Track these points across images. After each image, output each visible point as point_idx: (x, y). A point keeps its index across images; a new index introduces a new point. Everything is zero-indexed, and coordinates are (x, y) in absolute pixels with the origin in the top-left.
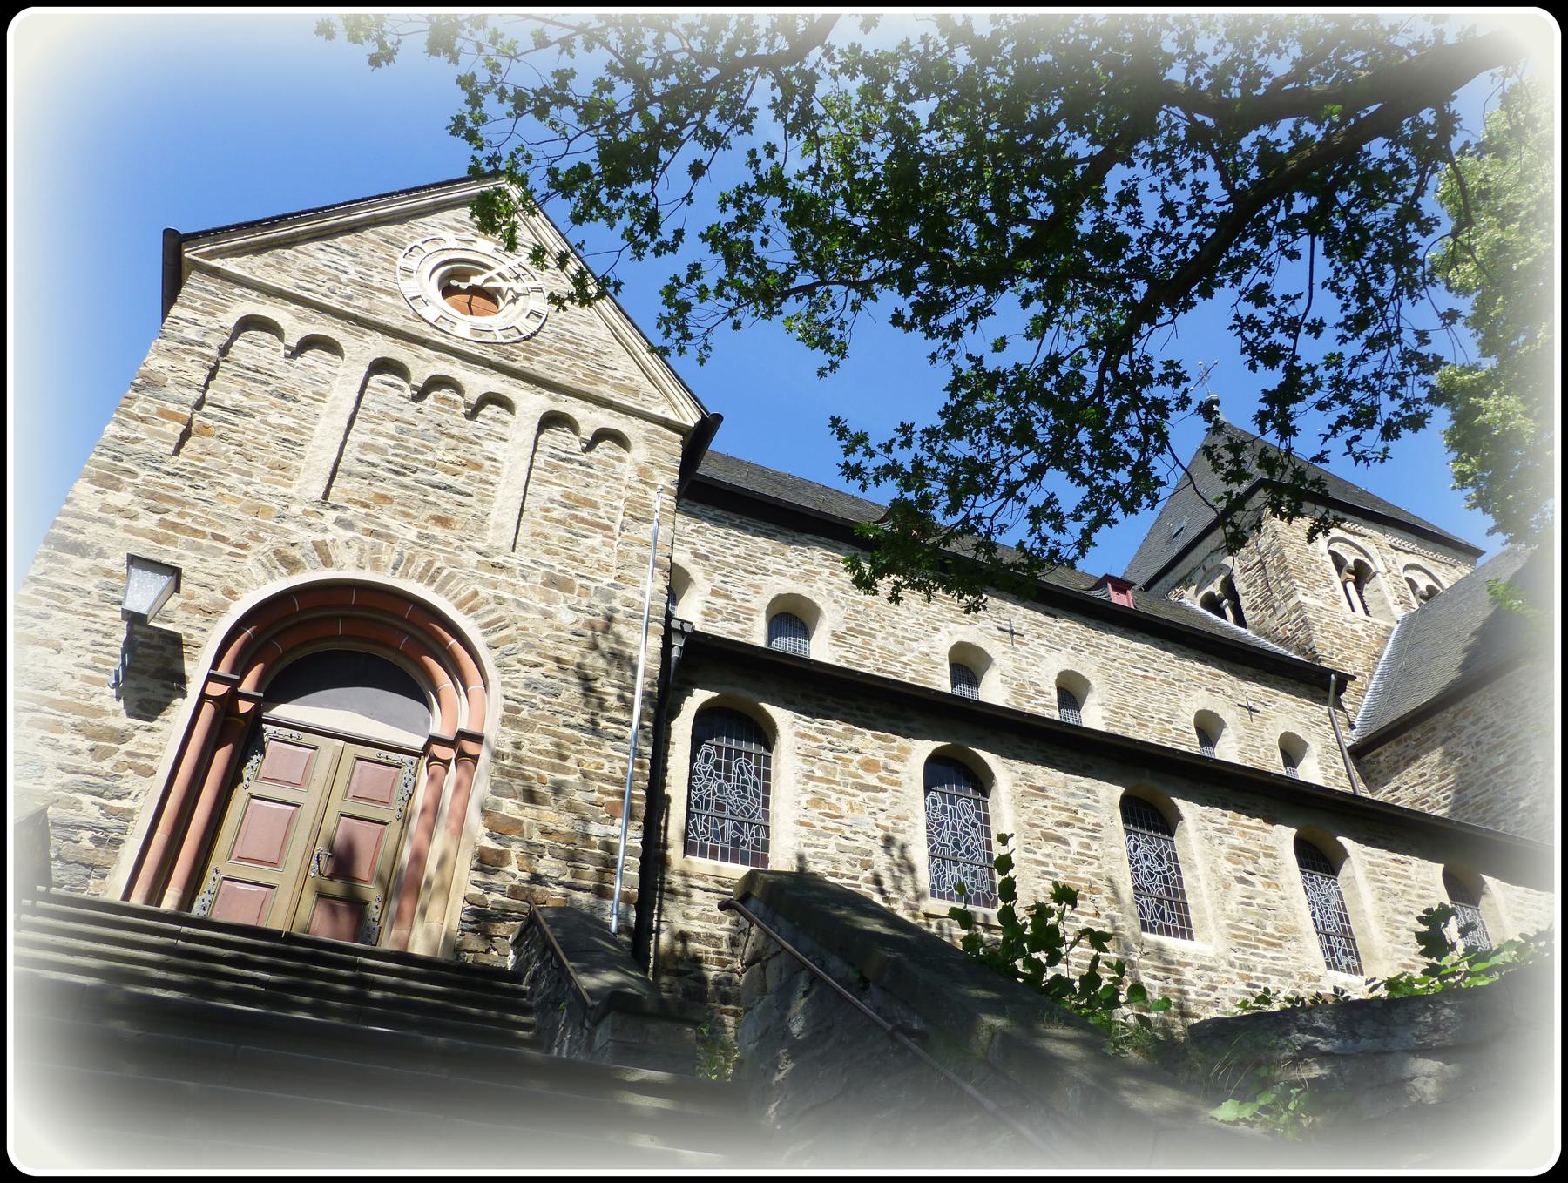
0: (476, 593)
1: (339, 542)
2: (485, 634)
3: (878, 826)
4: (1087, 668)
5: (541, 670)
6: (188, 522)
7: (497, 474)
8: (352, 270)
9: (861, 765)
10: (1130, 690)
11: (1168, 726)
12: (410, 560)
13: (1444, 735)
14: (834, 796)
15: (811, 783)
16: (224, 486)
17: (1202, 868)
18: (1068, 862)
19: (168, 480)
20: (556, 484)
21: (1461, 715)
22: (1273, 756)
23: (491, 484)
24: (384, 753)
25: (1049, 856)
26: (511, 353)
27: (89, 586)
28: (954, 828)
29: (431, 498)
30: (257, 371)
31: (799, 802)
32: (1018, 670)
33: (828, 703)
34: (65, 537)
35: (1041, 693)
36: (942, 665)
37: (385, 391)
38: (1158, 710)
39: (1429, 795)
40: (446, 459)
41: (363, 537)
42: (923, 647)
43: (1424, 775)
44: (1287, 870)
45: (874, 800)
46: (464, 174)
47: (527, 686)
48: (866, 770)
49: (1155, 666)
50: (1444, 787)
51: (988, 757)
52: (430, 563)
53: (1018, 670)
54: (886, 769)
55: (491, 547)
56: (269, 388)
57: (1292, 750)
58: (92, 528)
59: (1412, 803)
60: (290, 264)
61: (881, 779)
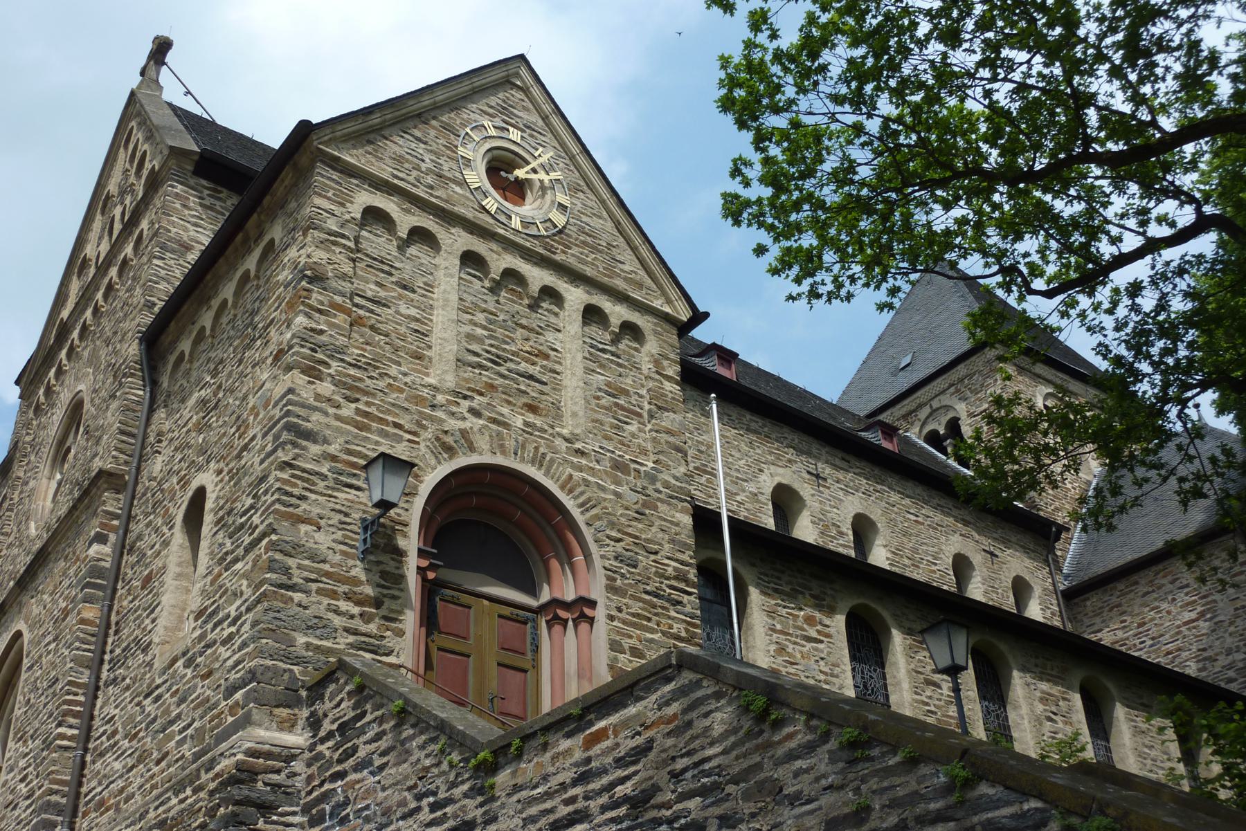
0: (571, 476)
1: (475, 429)
3: (821, 671)
4: (875, 514)
6: (372, 410)
7: (560, 363)
8: (427, 157)
9: (805, 620)
11: (934, 568)
12: (523, 446)
13: (1145, 590)
14: (791, 646)
15: (775, 635)
16: (390, 377)
17: (1024, 710)
18: (942, 703)
19: (352, 372)
20: (599, 373)
21: (1162, 574)
22: (1008, 597)
23: (558, 373)
24: (516, 611)
25: (930, 697)
26: (552, 246)
27: (324, 470)
28: (863, 673)
29: (522, 387)
30: (382, 262)
31: (769, 651)
32: (823, 512)
34: (300, 425)
35: (841, 534)
36: (767, 504)
37: (471, 283)
38: (926, 552)
39: (1127, 639)
40: (524, 349)
41: (490, 425)
43: (1125, 621)
44: (1077, 712)
45: (816, 649)
46: (963, 343)
47: (616, 558)
48: (809, 624)
50: (1140, 633)
51: (886, 615)
52: (536, 448)
53: (823, 512)
54: (821, 623)
56: (394, 279)
57: (1021, 588)
58: (315, 417)
59: (1112, 644)
60: (382, 150)
61: (819, 632)
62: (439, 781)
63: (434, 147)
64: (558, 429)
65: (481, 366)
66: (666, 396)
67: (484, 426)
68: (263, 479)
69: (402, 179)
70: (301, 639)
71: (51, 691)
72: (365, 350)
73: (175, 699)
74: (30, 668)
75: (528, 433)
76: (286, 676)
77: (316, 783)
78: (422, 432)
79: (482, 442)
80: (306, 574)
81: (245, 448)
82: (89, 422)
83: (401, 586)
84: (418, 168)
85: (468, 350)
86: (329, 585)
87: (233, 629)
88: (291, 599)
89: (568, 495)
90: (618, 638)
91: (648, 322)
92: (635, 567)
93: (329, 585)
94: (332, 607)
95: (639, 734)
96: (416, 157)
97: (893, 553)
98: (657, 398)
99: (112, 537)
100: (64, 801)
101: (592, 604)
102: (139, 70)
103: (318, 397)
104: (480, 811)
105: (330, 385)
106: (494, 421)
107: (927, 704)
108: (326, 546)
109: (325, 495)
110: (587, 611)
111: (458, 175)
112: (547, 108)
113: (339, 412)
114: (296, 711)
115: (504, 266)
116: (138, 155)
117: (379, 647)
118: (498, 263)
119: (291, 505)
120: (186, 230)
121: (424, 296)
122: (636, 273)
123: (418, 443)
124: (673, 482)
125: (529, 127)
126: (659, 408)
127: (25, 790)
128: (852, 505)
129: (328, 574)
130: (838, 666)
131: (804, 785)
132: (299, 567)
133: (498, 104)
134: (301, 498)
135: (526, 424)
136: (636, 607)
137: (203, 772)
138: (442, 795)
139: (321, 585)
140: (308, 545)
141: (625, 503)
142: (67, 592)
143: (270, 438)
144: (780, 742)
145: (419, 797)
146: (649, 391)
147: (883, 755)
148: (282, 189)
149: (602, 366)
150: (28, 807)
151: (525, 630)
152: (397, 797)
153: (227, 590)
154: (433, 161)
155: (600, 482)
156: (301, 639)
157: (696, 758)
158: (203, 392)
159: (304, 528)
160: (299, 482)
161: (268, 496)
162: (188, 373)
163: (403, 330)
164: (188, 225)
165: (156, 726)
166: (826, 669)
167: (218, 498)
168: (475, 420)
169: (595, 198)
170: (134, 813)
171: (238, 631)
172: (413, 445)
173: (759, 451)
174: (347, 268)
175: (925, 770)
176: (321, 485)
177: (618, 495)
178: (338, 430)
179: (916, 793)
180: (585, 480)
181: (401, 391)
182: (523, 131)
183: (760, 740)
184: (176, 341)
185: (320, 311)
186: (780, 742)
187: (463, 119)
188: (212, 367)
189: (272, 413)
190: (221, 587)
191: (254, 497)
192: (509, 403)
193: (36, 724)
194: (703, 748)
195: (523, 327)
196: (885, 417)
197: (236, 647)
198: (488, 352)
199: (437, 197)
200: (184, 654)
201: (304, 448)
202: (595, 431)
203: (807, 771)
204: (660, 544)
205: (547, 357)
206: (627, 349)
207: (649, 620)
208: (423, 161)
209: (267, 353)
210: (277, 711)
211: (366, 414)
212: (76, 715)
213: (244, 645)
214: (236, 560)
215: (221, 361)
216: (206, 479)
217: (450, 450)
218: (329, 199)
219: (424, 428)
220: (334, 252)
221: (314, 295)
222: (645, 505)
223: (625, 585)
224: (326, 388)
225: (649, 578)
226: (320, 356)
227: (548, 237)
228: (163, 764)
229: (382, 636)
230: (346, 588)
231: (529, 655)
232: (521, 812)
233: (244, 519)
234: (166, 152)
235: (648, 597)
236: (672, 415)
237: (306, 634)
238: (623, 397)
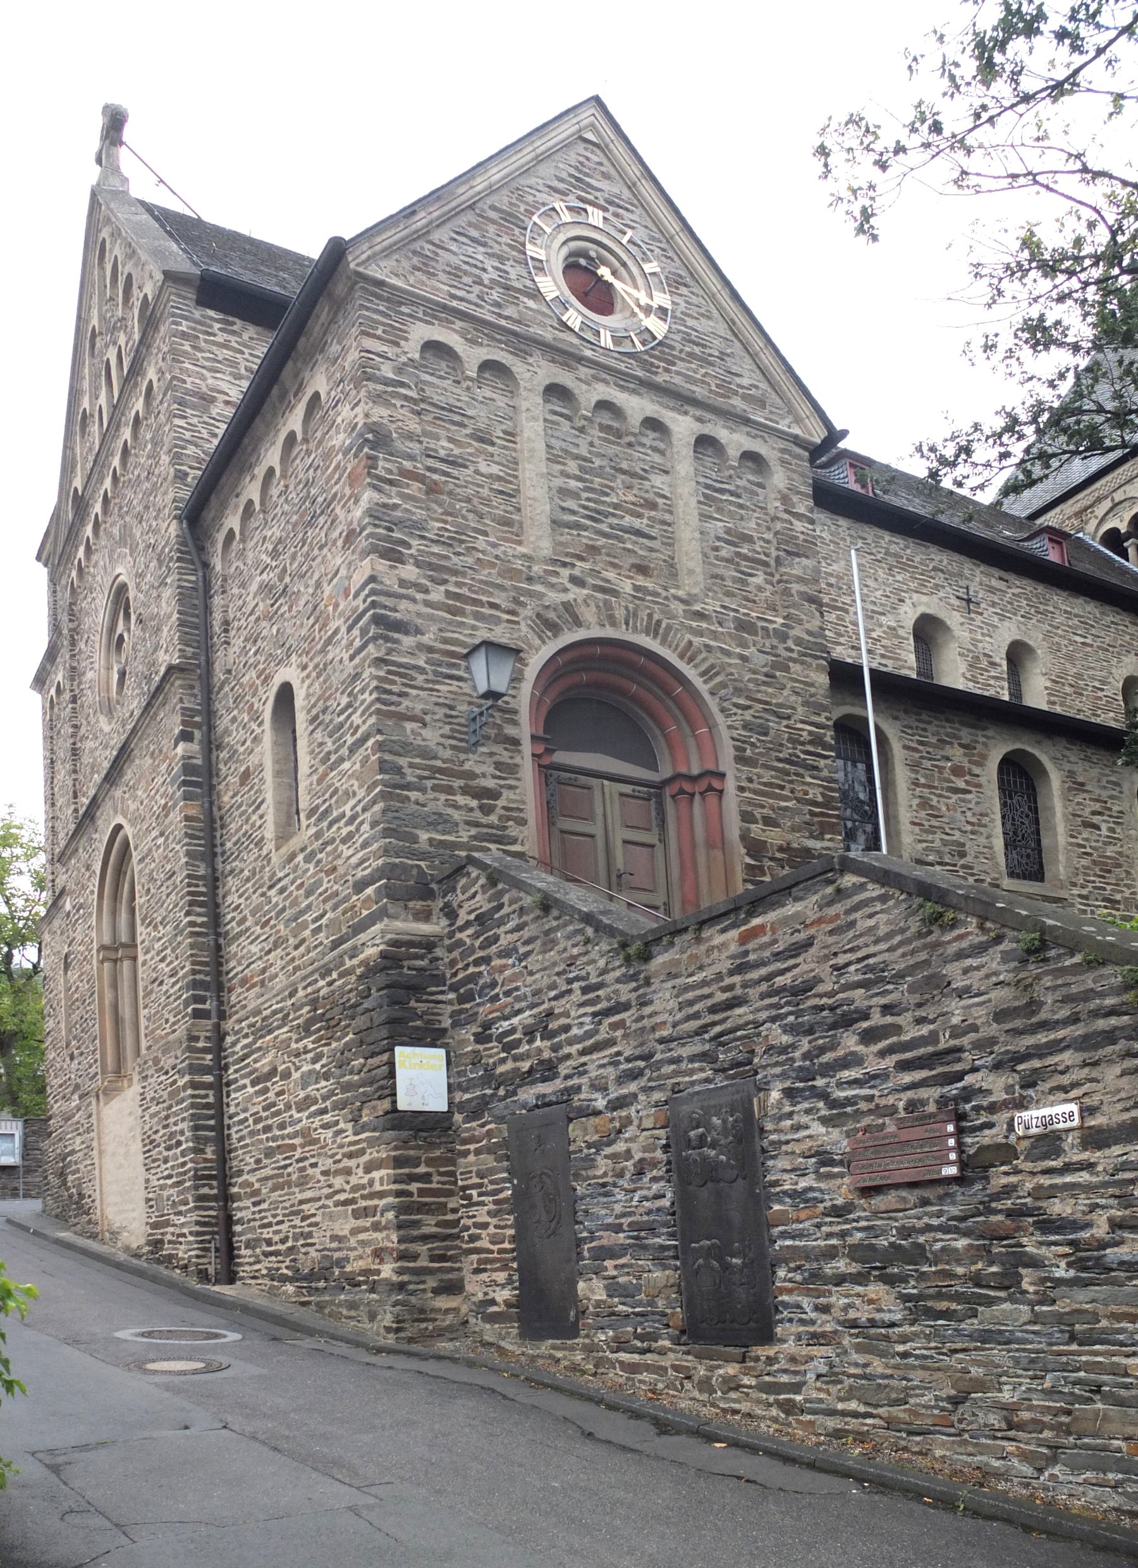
0: (690, 643)
2: (705, 682)
4: (1035, 639)
5: (751, 711)
6: (464, 591)
10: (1070, 658)
11: (1100, 694)
12: (635, 615)
14: (935, 799)
19: (436, 549)
23: (669, 525)
25: (1087, 840)
26: (652, 364)
27: (421, 663)
30: (451, 411)
33: (924, 717)
34: (387, 617)
35: (993, 664)
38: (1093, 678)
42: (888, 621)
45: (963, 800)
47: (745, 727)
49: (1093, 631)
51: (1044, 759)
52: (650, 616)
55: (689, 594)
56: (468, 431)
58: (403, 605)
61: (967, 782)
62: (589, 968)
63: (496, 249)
64: (673, 591)
65: (578, 526)
66: (797, 538)
67: (589, 596)
68: (356, 676)
69: (462, 299)
70: (424, 836)
71: (170, 882)
72: (446, 522)
73: (302, 892)
74: (141, 860)
76: (415, 872)
77: (460, 966)
78: (520, 610)
79: (589, 614)
81: (329, 641)
82: (141, 610)
85: (563, 509)
86: (444, 781)
87: (352, 828)
88: (408, 798)
92: (766, 734)
93: (444, 781)
95: (799, 931)
96: (476, 266)
97: (1054, 681)
98: (787, 543)
99: (197, 734)
100: (208, 978)
101: (722, 776)
102: (93, 157)
103: (403, 583)
104: (634, 995)
105: (413, 568)
106: (597, 588)
107: (1084, 847)
111: (529, 283)
112: (634, 171)
114: (429, 902)
115: (595, 398)
116: (121, 281)
117: (502, 836)
119: (393, 704)
120: (203, 378)
121: (504, 447)
122: (757, 387)
123: (518, 623)
124: (807, 637)
125: (611, 203)
127: (167, 970)
128: (1008, 632)
129: (441, 771)
130: (987, 815)
131: (974, 980)
132: (411, 765)
134: (402, 695)
135: (637, 588)
136: (767, 776)
137: (346, 958)
138: (594, 980)
140: (415, 742)
142: (162, 790)
143: (356, 632)
144: (949, 942)
145: (570, 982)
146: (776, 533)
147: (1059, 956)
148: (318, 328)
149: (719, 510)
150: (174, 984)
152: (546, 981)
153: (336, 791)
154: (497, 269)
156: (424, 836)
157: (860, 954)
158: (265, 576)
159: (409, 726)
160: (396, 678)
161: (366, 695)
162: (242, 554)
163: (485, 492)
164: (204, 372)
165: (288, 914)
166: (974, 820)
167: (308, 696)
169: (701, 292)
170: (282, 991)
171: (358, 830)
173: (899, 578)
174: (413, 425)
175: (1108, 970)
176: (420, 679)
177: (744, 659)
178: (431, 618)
179: (1092, 990)
180: (707, 646)
182: (605, 210)
183: (929, 939)
184: (220, 515)
185: (391, 482)
186: (949, 942)
187: (527, 203)
188: (271, 547)
189: (354, 604)
190: (330, 786)
191: (349, 695)
193: (163, 912)
194: (867, 946)
195: (624, 472)
196: (1051, 519)
197: (358, 845)
198: (585, 507)
199: (507, 318)
200: (303, 850)
201: (396, 641)
203: (978, 968)
204: (793, 708)
205: (653, 506)
206: (749, 486)
207: (782, 788)
208: (484, 270)
209: (335, 534)
210: (411, 904)
211: (457, 597)
212: (201, 904)
213: (365, 845)
214: (342, 760)
215: (280, 541)
216: (289, 673)
217: (554, 628)
218: (379, 338)
219: (523, 605)
220: (394, 405)
221: (381, 463)
224: (409, 572)
225: (781, 745)
226: (397, 535)
228: (302, 949)
230: (461, 782)
232: (677, 996)
233: (342, 718)
234: (159, 277)
235: (781, 765)
236: (804, 561)
238: (746, 546)
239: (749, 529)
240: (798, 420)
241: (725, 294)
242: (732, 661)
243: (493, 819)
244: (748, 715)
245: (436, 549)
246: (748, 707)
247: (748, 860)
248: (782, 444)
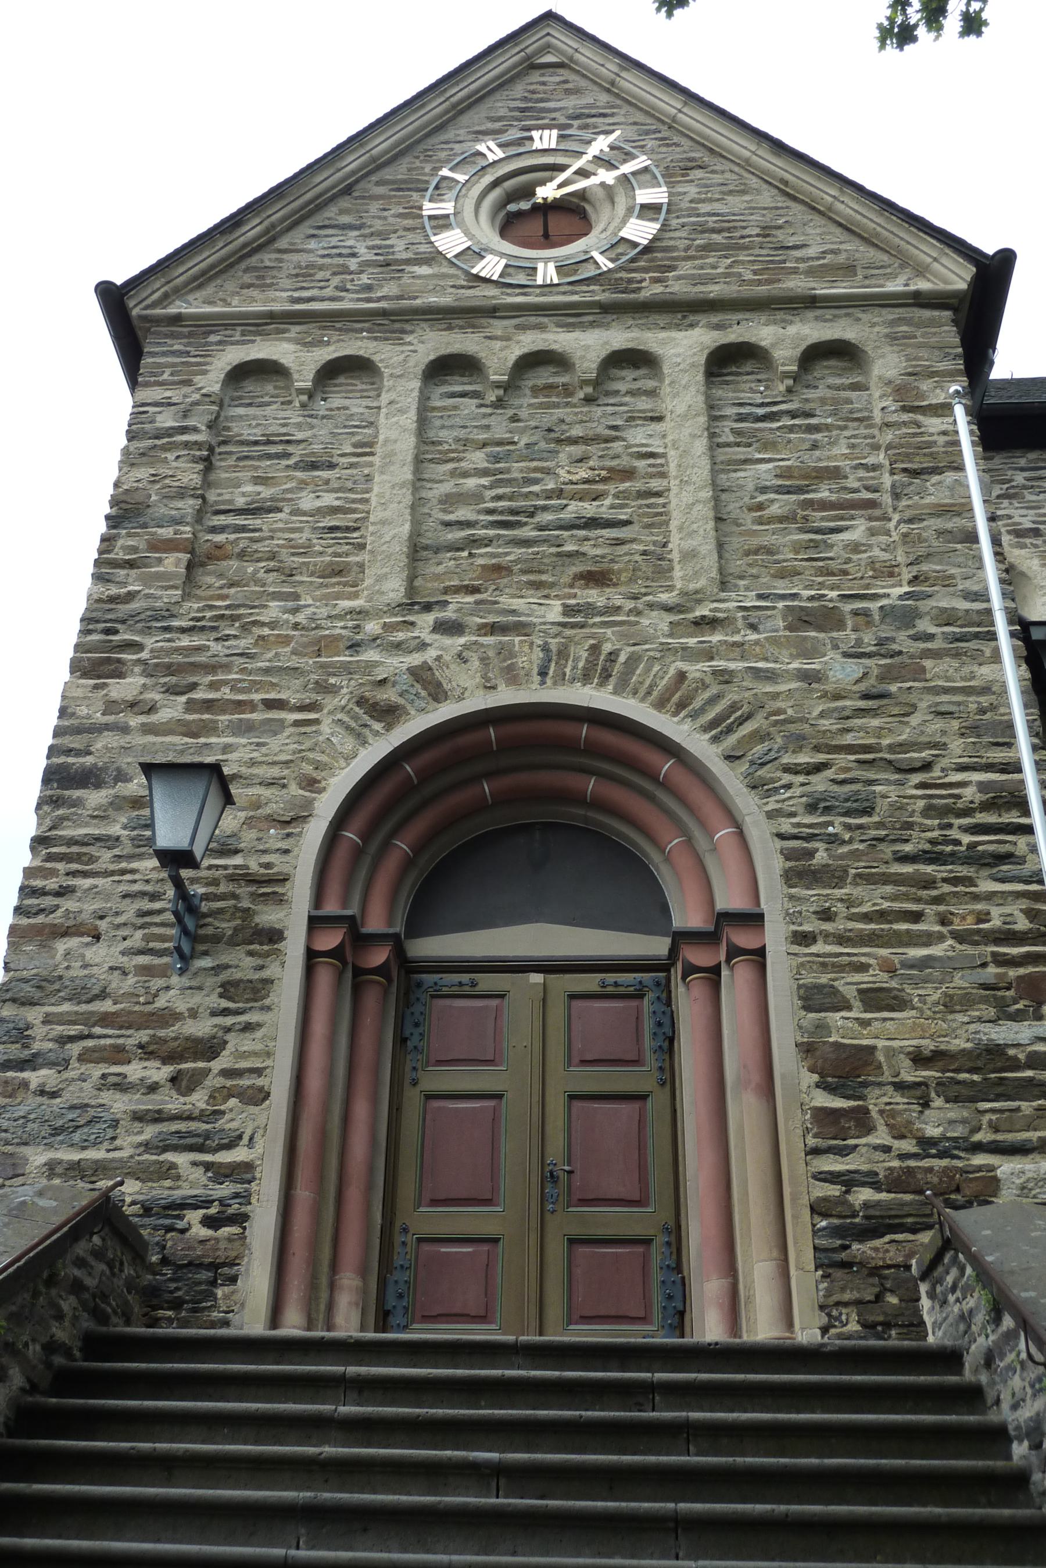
0: (682, 676)
1: (447, 658)
2: (715, 739)
5: (829, 773)
16: (263, 624)
19: (185, 641)
23: (658, 494)
24: (611, 977)
26: (630, 281)
29: (569, 547)
30: (269, 442)
37: (455, 408)
47: (812, 808)
52: (595, 649)
60: (275, 273)
66: (930, 444)
75: (573, 626)
80: (59, 1029)
83: (267, 1002)
84: (345, 270)
85: (448, 524)
86: (108, 1037)
88: (25, 1084)
89: (675, 714)
90: (824, 979)
91: (874, 325)
92: (868, 812)
93: (108, 1037)
94: (112, 1079)
108: (106, 966)
109: (113, 873)
110: (743, 939)
112: (610, 68)
113: (153, 718)
117: (207, 1136)
118: (502, 355)
123: (317, 722)
126: (915, 473)
129: (105, 1020)
133: (511, 110)
139: (90, 1043)
140: (73, 973)
141: (829, 687)
151: (639, 1011)
155: (761, 665)
159: (61, 946)
163: (301, 538)
168: (447, 641)
172: (303, 730)
176: (105, 858)
181: (286, 640)
185: (131, 564)
192: (537, 585)
198: (490, 512)
201: (77, 803)
202: (754, 571)
204: (935, 745)
206: (829, 393)
207: (916, 917)
222: (886, 676)
223: (842, 857)
227: (621, 268)
229: (215, 1112)
230: (143, 1036)
231: (651, 1061)
235: (908, 869)
237: (50, 1146)
239: (834, 458)
240: (921, 271)
241: (764, 152)
242: (782, 688)
243: (198, 1100)
244: (819, 783)
245: (185, 641)
246: (819, 768)
247: (824, 1100)
248: (890, 314)
